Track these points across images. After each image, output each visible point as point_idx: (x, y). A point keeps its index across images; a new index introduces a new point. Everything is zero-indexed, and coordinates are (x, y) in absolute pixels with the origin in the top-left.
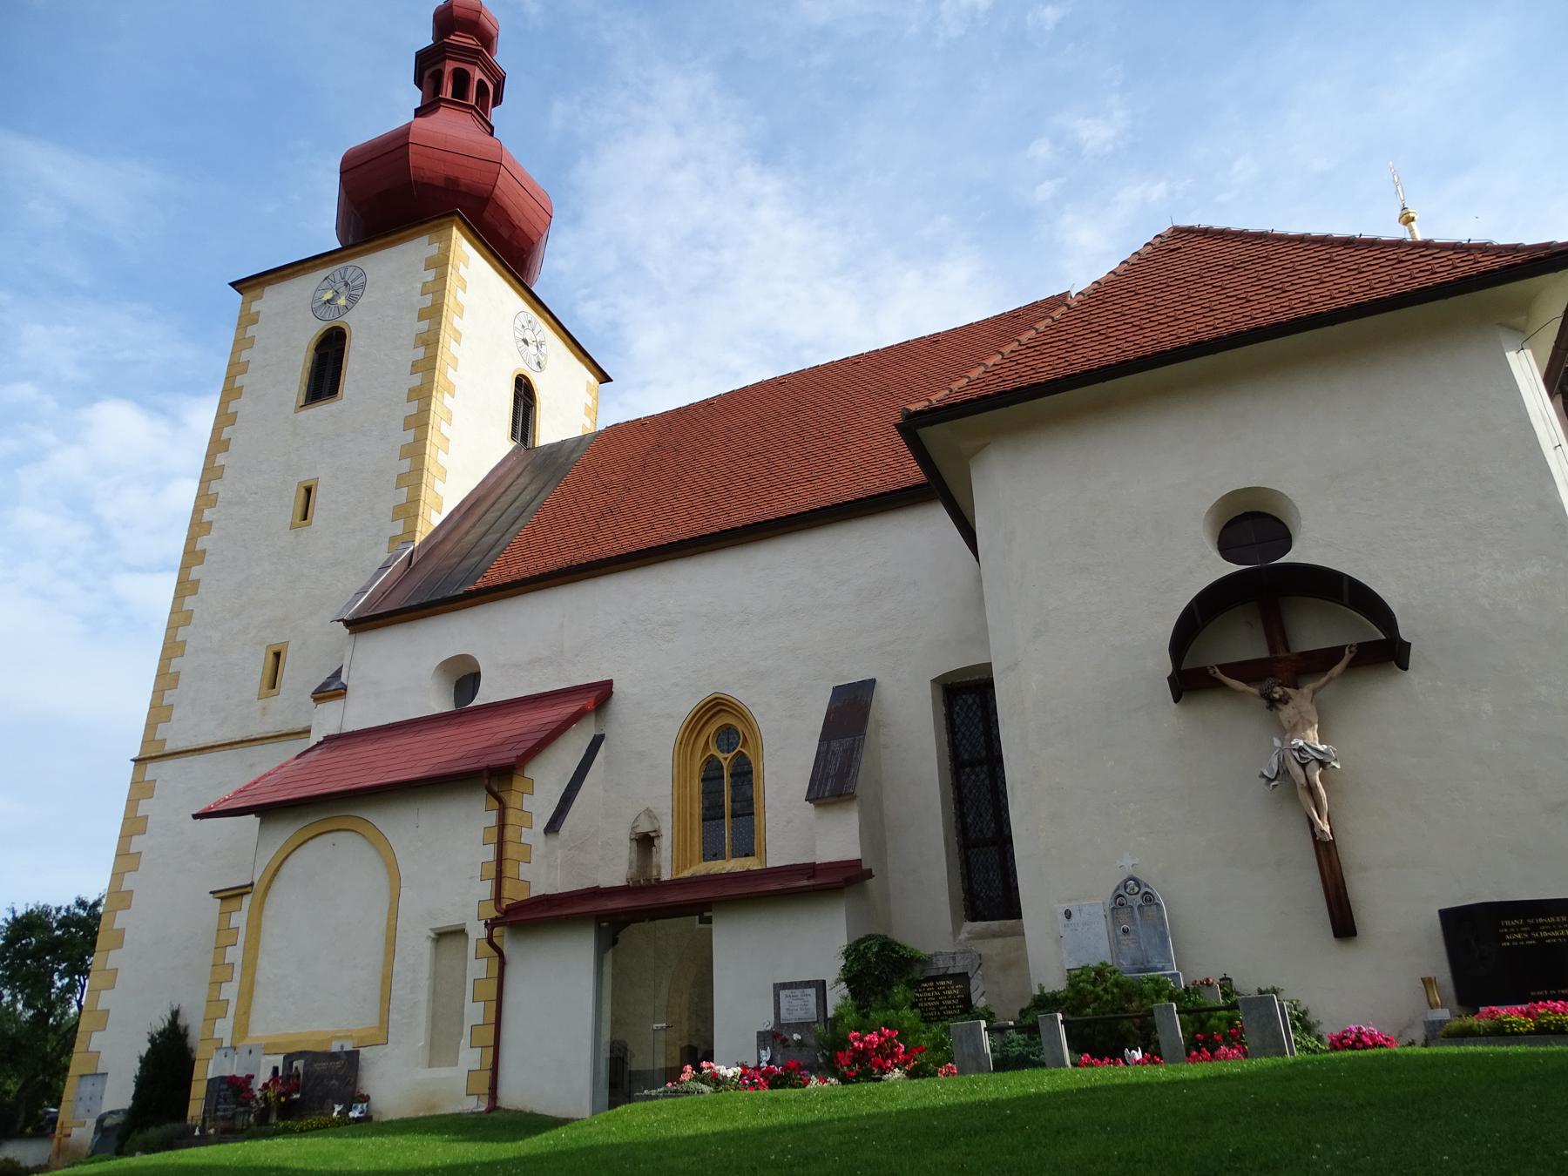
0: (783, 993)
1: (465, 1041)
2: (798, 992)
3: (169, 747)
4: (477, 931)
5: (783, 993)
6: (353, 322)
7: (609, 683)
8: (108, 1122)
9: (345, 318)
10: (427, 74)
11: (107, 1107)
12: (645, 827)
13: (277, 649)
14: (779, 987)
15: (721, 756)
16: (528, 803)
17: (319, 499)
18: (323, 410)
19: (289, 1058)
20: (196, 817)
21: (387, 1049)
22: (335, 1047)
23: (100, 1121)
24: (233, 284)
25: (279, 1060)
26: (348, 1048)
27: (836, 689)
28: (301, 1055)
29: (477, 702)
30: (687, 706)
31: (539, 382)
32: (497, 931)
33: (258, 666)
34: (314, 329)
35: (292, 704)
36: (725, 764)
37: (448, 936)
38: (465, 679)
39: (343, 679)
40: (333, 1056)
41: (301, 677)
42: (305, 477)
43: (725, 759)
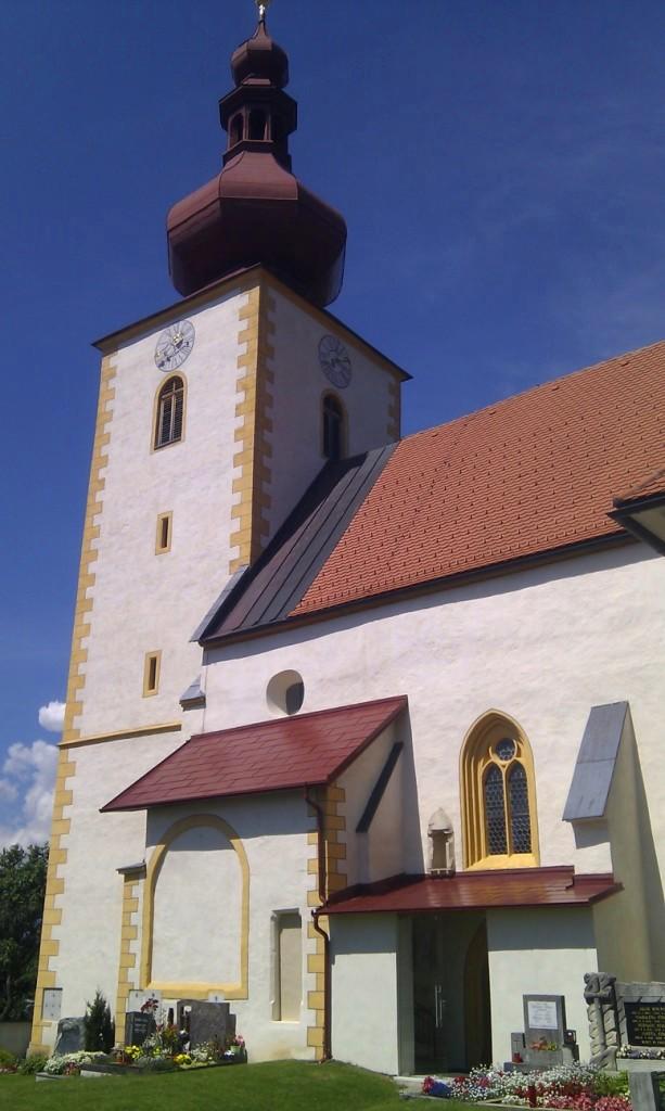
0: (530, 1003)
1: (303, 1003)
2: (542, 1004)
3: (82, 738)
4: (307, 918)
5: (530, 1003)
6: (189, 371)
7: (405, 698)
8: (65, 1026)
9: (181, 369)
10: (230, 120)
11: (65, 1015)
12: (439, 826)
13: (153, 656)
14: (527, 998)
15: (500, 762)
16: (342, 809)
17: (176, 530)
18: (171, 451)
19: (181, 1004)
20: (101, 811)
21: (247, 1003)
22: (211, 1000)
23: (60, 1025)
24: (94, 345)
25: (173, 1004)
26: (221, 1001)
27: (594, 709)
28: (189, 1002)
29: (302, 711)
30: (469, 721)
31: (347, 397)
32: (321, 918)
33: (140, 671)
34: (158, 378)
35: (164, 707)
36: (504, 771)
37: (286, 920)
38: (290, 690)
39: (202, 688)
40: (211, 1006)
41: (174, 684)
42: (163, 510)
43: (503, 764)
